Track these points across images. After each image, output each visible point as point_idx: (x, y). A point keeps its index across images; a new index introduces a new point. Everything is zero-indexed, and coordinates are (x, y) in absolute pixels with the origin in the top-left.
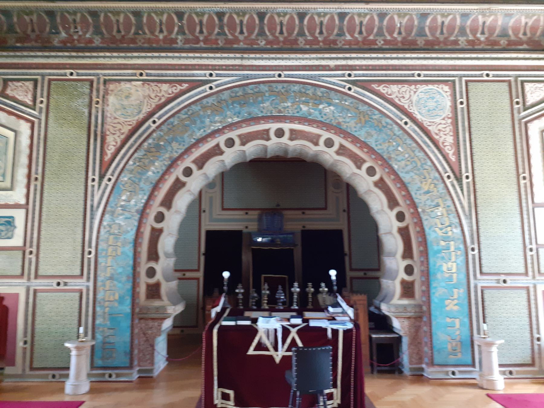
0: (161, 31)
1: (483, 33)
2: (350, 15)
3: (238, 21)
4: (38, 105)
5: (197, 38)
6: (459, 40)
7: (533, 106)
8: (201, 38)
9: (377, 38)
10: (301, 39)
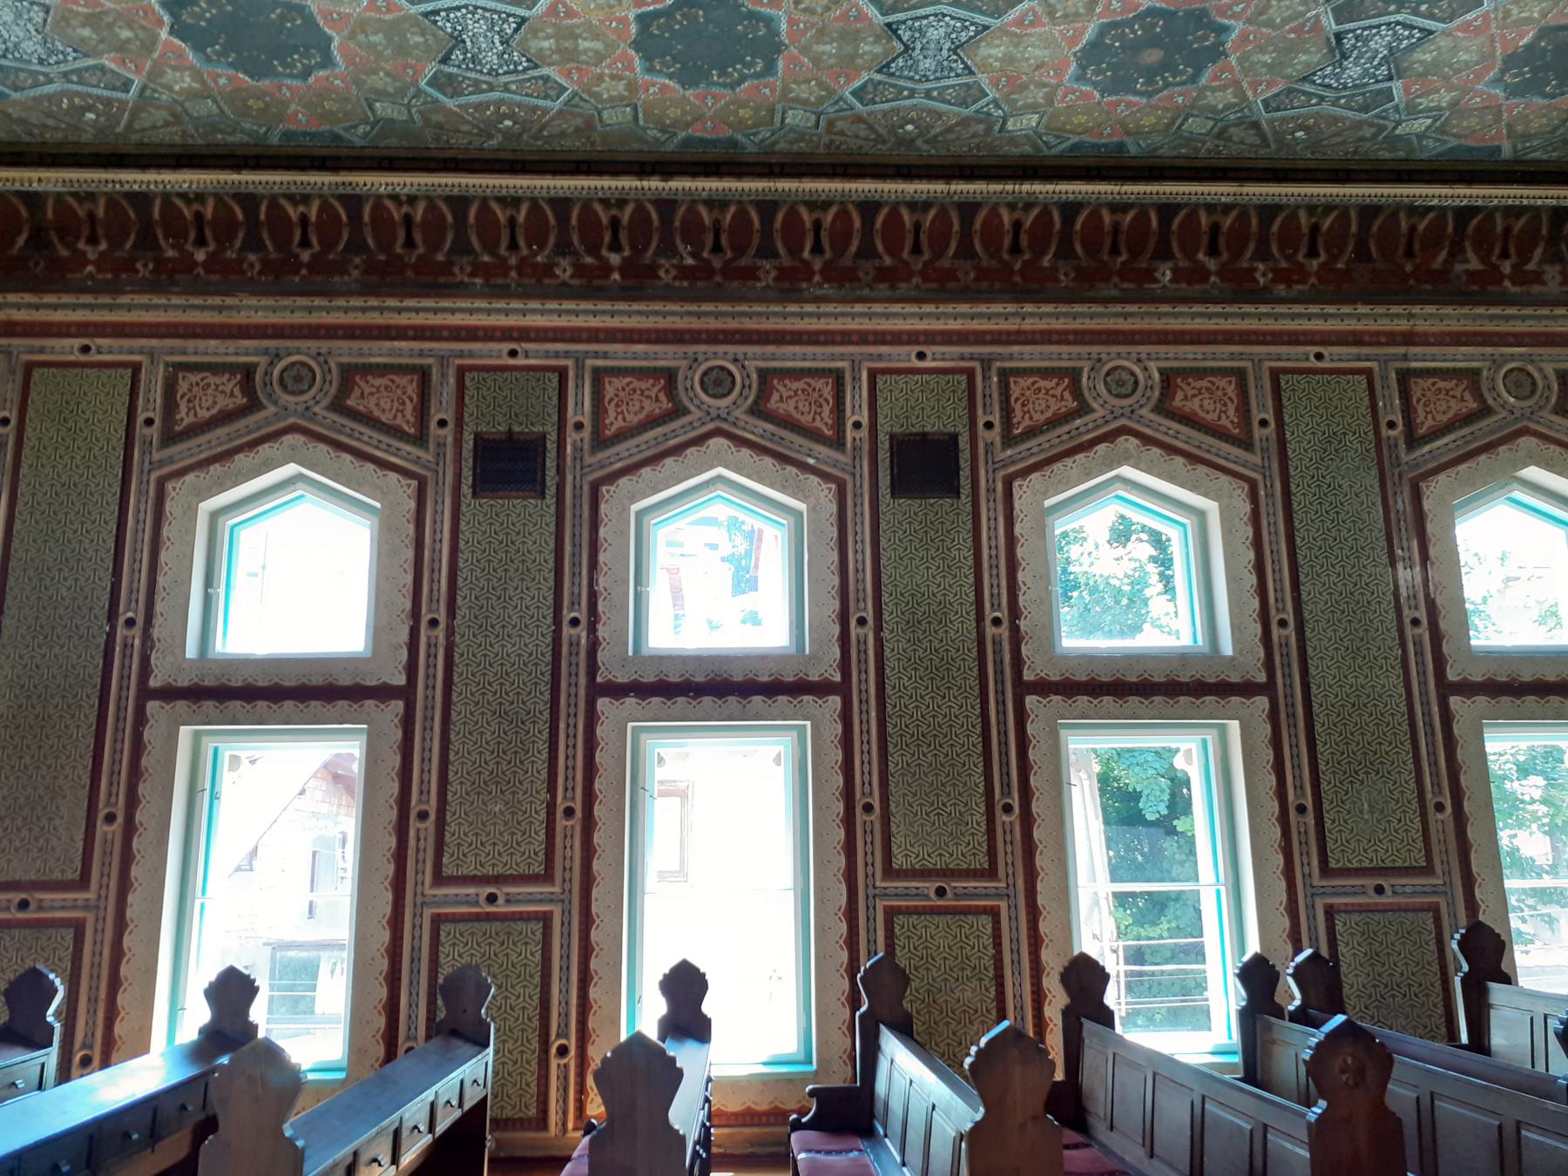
0: (201, 242)
1: (1213, 251)
2: (983, 213)
3: (605, 220)
4: (1258, 433)
5: (504, 260)
6: (659, 267)
7: (1031, 433)
8: (513, 261)
9: (759, 262)
10: (565, 262)
